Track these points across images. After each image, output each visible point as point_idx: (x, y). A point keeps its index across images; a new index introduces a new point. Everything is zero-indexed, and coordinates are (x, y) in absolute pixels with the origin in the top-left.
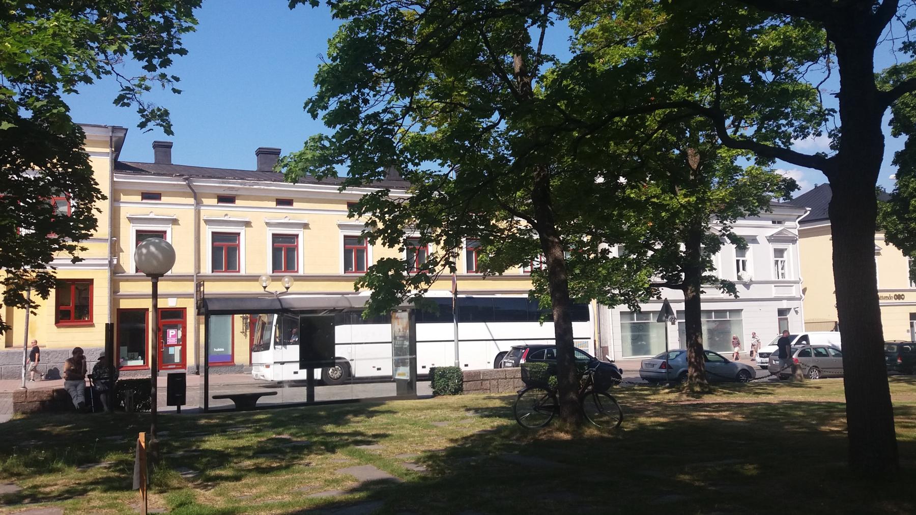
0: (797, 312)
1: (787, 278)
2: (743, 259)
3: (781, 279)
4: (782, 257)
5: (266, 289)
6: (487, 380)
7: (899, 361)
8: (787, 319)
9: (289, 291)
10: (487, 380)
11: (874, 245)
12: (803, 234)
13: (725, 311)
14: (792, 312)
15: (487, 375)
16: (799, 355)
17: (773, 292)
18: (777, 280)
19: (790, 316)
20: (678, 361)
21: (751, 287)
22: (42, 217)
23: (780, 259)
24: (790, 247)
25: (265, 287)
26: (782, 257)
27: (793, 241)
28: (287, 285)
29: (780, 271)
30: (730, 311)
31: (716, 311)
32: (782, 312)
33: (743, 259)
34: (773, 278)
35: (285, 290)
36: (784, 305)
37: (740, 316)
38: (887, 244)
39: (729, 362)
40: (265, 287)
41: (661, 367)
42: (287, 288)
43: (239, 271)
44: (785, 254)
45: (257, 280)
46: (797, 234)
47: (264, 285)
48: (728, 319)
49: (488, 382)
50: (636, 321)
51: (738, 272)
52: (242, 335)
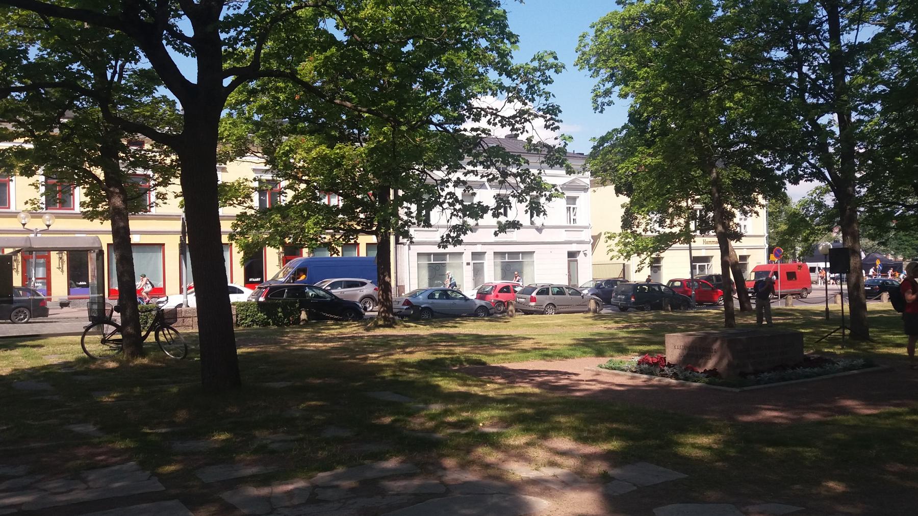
0: (585, 254)
1: (578, 223)
2: (574, 206)
3: (572, 224)
4: (575, 204)
5: (26, 227)
6: (190, 317)
7: (633, 299)
8: (577, 261)
9: (50, 228)
10: (190, 317)
11: (186, 212)
12: (593, 184)
13: (519, 253)
14: (581, 254)
15: (189, 313)
16: (537, 294)
17: (563, 236)
18: (569, 225)
19: (580, 258)
20: (420, 299)
21: (543, 231)
22: (892, 30)
23: (572, 206)
24: (581, 195)
25: (24, 225)
26: (575, 204)
27: (585, 190)
28: (48, 223)
29: (572, 218)
30: (523, 253)
31: (510, 253)
32: (572, 255)
33: (574, 206)
34: (565, 223)
35: (46, 228)
36: (574, 248)
37: (461, 258)
38: (618, 196)
39: (469, 299)
40: (24, 225)
41: (404, 305)
42: (48, 226)
43: (9, 208)
44: (578, 201)
45: (16, 217)
46: (589, 183)
47: (23, 222)
48: (521, 260)
49: (191, 319)
50: (432, 262)
51: (531, 218)
52: (59, 272)
